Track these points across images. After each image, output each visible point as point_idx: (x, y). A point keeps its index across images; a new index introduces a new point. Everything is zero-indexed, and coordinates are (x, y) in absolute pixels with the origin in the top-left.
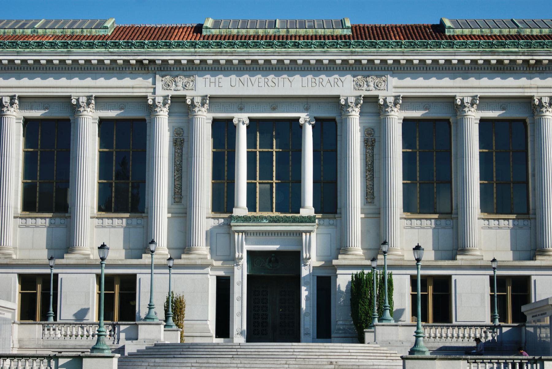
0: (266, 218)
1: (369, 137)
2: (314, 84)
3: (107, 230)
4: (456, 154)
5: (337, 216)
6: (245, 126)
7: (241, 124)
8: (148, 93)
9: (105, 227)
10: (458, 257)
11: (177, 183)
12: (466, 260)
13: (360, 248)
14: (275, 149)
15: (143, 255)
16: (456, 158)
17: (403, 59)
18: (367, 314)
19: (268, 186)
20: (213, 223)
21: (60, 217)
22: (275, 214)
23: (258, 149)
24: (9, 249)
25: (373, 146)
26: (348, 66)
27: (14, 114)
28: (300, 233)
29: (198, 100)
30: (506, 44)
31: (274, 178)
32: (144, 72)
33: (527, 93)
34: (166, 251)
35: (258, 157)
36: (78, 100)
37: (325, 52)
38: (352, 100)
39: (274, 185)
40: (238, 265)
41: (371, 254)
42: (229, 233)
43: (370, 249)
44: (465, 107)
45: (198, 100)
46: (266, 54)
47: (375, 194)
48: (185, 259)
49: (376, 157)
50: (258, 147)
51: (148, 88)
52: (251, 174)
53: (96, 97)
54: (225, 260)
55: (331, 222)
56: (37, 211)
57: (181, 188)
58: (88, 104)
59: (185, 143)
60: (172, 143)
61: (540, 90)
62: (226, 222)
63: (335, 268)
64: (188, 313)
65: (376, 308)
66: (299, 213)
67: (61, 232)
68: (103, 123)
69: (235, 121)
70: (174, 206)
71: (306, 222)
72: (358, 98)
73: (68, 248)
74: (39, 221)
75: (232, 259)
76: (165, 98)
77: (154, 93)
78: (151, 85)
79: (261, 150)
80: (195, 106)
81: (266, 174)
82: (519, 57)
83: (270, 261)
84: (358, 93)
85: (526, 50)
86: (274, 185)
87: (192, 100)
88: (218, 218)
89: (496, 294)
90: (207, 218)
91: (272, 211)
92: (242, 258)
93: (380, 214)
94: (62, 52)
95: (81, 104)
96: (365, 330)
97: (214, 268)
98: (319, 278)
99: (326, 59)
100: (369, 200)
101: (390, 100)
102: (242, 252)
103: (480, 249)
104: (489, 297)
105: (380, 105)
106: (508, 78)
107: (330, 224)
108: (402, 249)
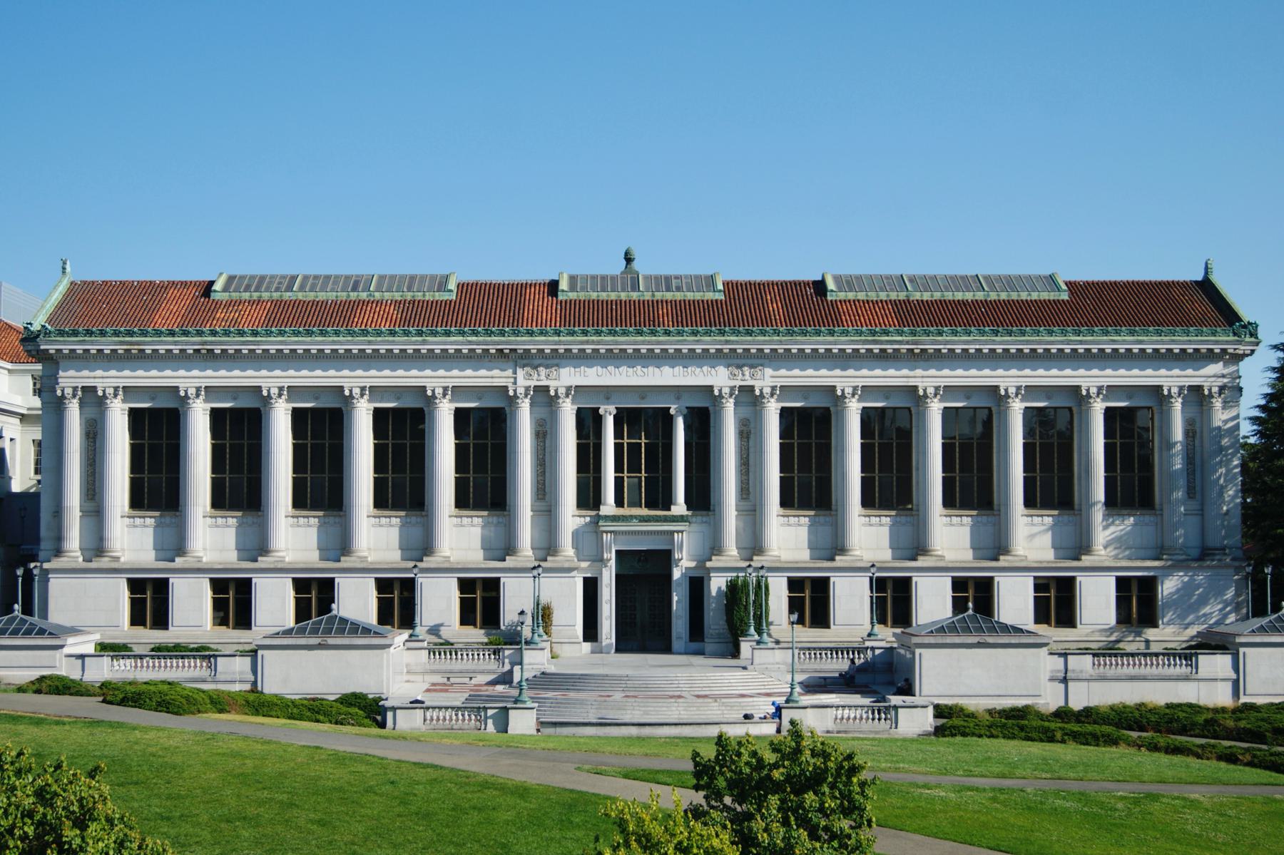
0: (635, 517)
1: (745, 428)
2: (686, 374)
3: (139, 529)
4: (837, 447)
5: (710, 513)
6: (612, 416)
7: (608, 414)
8: (507, 382)
9: (300, 526)
10: (838, 558)
11: (540, 478)
12: (846, 561)
13: (735, 548)
14: (643, 441)
15: (507, 557)
16: (999, 452)
17: (781, 348)
18: (742, 621)
19: (636, 480)
20: (581, 521)
21: (416, 516)
22: (644, 512)
23: (626, 441)
24: (363, 551)
25: (748, 438)
26: (722, 355)
27: (201, 405)
28: (672, 533)
29: (562, 391)
30: (889, 332)
31: (643, 472)
32: (503, 360)
33: (912, 382)
34: (530, 553)
35: (626, 449)
36: (433, 391)
37: (698, 341)
38: (726, 391)
39: (643, 479)
40: (606, 566)
41: (541, 554)
42: (596, 532)
43: (745, 548)
44: (846, 397)
45: (562, 391)
46: (635, 343)
47: (751, 490)
48: (551, 562)
49: (751, 450)
50: (626, 438)
51: (509, 377)
52: (619, 468)
53: (124, 387)
54: (594, 561)
55: (704, 519)
56: (796, 506)
57: (544, 484)
58: (444, 395)
59: (548, 436)
60: (84, 436)
61: (925, 380)
62: (593, 520)
63: (709, 570)
64: (557, 618)
65: (752, 614)
66: (669, 510)
67: (417, 532)
68: (784, 413)
69: (601, 411)
70: (86, 504)
71: (677, 521)
72: (732, 388)
73: (426, 549)
74: (884, 519)
75: (601, 561)
76: (527, 389)
77: (515, 383)
78: (511, 375)
79: (629, 441)
80: (559, 397)
81: (635, 468)
82: (725, 347)
83: (639, 560)
84: (733, 383)
85: (910, 338)
86: (643, 479)
87: (556, 391)
88: (584, 516)
89: (875, 595)
90: (573, 516)
91: (641, 507)
92: (610, 559)
93: (755, 511)
94: (417, 341)
95: (437, 395)
96: (740, 639)
97: (584, 570)
98: (691, 578)
99: (699, 348)
100: (90, 497)
101: (767, 391)
102: (610, 553)
103: (861, 548)
104: (951, 598)
105: (919, 396)
106: (1207, 366)
107: (703, 522)
108: (780, 548)
